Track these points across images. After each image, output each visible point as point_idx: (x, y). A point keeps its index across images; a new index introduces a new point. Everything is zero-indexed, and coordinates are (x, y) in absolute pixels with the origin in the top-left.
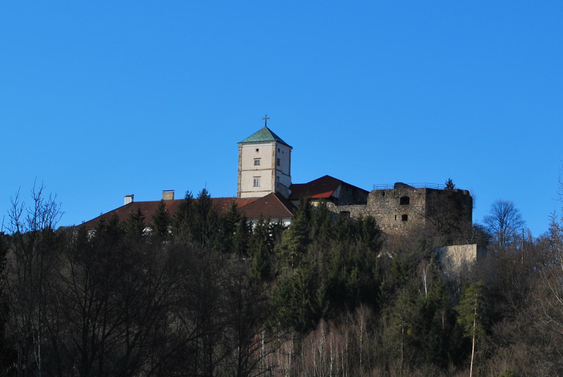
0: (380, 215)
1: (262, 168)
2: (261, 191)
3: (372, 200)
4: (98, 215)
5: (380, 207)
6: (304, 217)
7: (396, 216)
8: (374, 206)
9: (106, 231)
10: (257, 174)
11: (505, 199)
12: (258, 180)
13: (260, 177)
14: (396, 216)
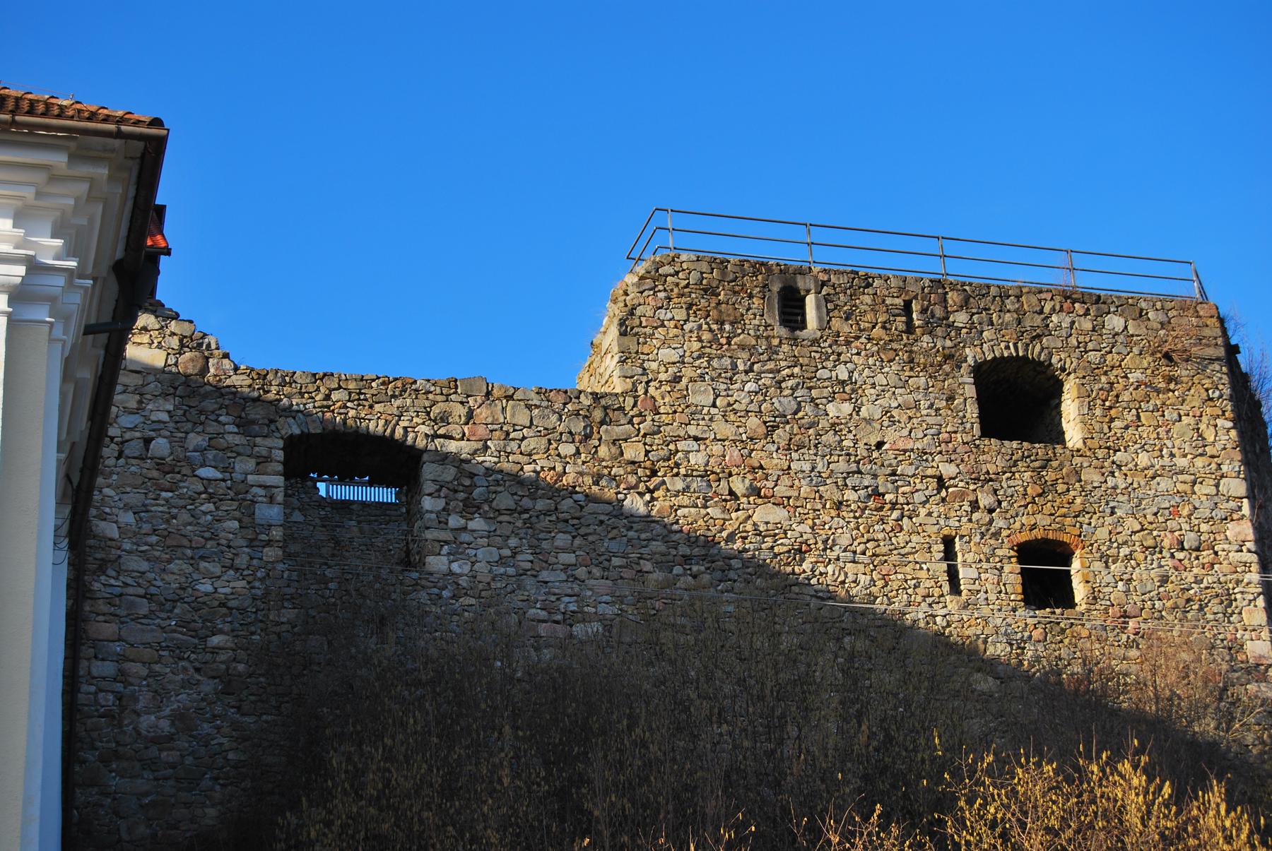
0: (778, 515)
3: (668, 354)
4: (161, 268)
5: (771, 429)
6: (133, 334)
7: (948, 542)
8: (695, 413)
14: (948, 542)
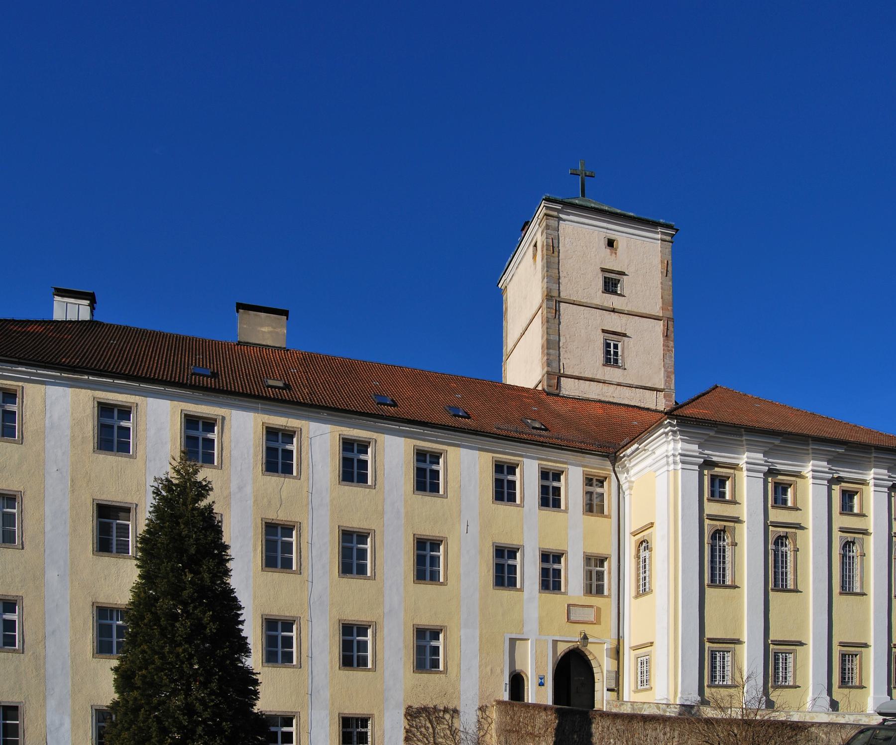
1: (626, 308)
2: (630, 386)
9: (214, 633)
10: (615, 323)
11: (213, 485)
12: (616, 347)
13: (630, 337)
